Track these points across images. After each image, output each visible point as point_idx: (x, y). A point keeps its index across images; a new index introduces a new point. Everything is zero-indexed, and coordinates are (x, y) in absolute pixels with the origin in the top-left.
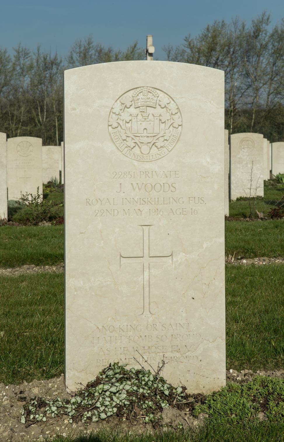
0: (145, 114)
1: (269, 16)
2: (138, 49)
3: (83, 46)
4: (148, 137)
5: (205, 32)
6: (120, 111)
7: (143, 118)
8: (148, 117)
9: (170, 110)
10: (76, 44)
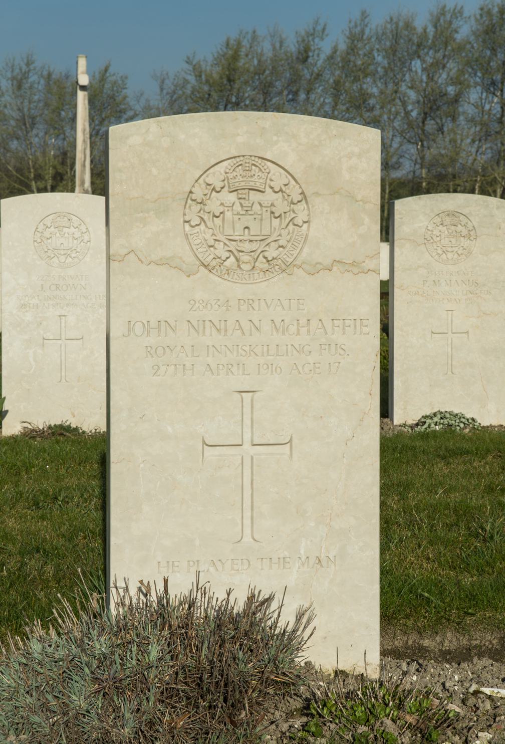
0: (247, 202)
1: (325, 25)
2: (110, 76)
3: (18, 67)
4: (251, 241)
5: (225, 50)
6: (203, 196)
7: (242, 210)
8: (252, 207)
9: (289, 196)
10: (7, 64)
